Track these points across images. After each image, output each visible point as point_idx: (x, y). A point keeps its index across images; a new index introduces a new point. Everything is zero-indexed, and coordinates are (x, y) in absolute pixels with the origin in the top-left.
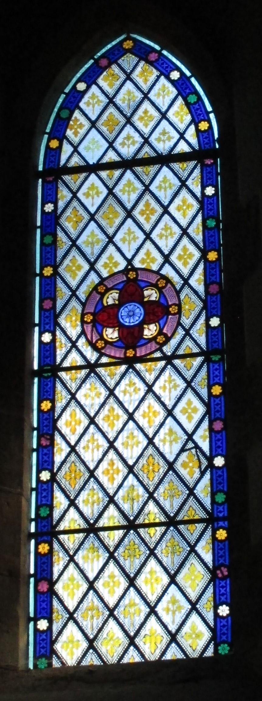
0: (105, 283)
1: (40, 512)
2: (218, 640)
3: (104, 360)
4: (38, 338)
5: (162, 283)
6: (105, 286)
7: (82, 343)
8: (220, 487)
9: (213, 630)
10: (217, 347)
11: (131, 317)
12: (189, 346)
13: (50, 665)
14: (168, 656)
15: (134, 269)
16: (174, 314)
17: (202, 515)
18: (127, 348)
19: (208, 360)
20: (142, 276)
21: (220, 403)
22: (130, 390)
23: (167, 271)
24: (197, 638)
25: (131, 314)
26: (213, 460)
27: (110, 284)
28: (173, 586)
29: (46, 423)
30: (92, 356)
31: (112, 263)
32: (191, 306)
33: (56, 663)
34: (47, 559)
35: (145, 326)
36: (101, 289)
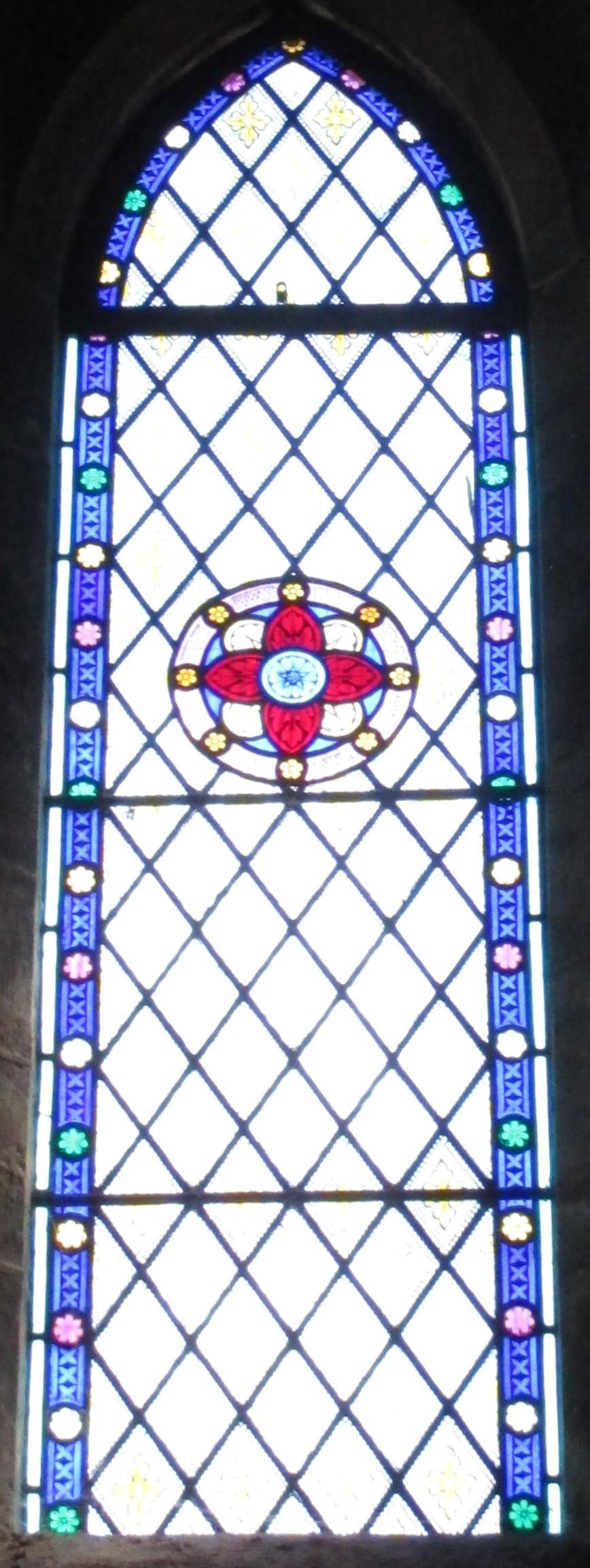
0: (228, 600)
1: (66, 969)
2: (495, 937)
3: (228, 785)
4: (63, 711)
5: (370, 615)
6: (228, 608)
7: (171, 740)
8: (498, 574)
9: (473, 432)
10: (520, 1184)
11: (292, 670)
12: (435, 773)
13: (82, 1527)
14: (385, 1527)
15: (303, 581)
16: (402, 688)
17: (474, 1183)
18: (282, 756)
19: (482, 806)
20: (317, 594)
21: (512, 901)
22: (293, 857)
23: (386, 591)
24: (457, 1498)
25: (294, 677)
26: (483, 549)
27: (239, 604)
28: (397, 1498)
29: (76, 1098)
30: (199, 772)
31: (248, 561)
32: (445, 675)
33: (96, 1527)
34: (79, 1262)
35: (327, 707)
36: (219, 614)
